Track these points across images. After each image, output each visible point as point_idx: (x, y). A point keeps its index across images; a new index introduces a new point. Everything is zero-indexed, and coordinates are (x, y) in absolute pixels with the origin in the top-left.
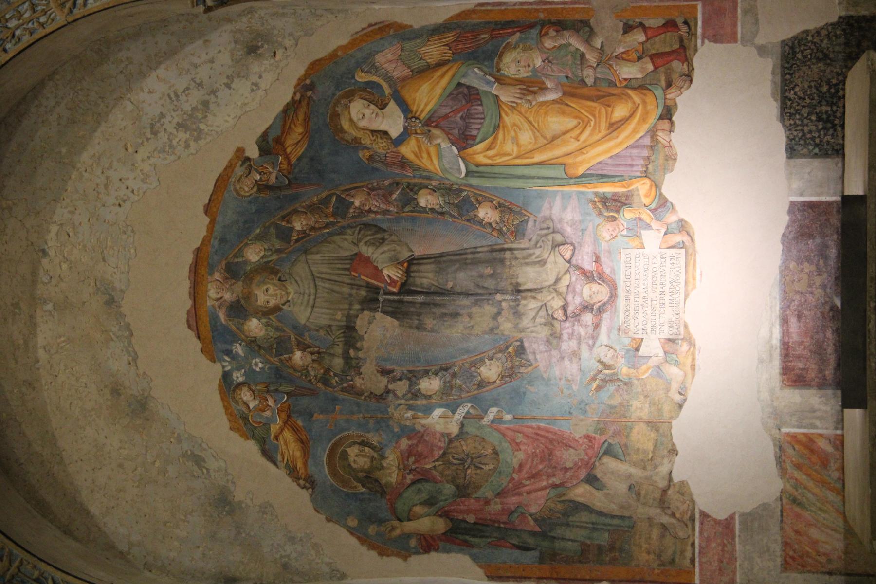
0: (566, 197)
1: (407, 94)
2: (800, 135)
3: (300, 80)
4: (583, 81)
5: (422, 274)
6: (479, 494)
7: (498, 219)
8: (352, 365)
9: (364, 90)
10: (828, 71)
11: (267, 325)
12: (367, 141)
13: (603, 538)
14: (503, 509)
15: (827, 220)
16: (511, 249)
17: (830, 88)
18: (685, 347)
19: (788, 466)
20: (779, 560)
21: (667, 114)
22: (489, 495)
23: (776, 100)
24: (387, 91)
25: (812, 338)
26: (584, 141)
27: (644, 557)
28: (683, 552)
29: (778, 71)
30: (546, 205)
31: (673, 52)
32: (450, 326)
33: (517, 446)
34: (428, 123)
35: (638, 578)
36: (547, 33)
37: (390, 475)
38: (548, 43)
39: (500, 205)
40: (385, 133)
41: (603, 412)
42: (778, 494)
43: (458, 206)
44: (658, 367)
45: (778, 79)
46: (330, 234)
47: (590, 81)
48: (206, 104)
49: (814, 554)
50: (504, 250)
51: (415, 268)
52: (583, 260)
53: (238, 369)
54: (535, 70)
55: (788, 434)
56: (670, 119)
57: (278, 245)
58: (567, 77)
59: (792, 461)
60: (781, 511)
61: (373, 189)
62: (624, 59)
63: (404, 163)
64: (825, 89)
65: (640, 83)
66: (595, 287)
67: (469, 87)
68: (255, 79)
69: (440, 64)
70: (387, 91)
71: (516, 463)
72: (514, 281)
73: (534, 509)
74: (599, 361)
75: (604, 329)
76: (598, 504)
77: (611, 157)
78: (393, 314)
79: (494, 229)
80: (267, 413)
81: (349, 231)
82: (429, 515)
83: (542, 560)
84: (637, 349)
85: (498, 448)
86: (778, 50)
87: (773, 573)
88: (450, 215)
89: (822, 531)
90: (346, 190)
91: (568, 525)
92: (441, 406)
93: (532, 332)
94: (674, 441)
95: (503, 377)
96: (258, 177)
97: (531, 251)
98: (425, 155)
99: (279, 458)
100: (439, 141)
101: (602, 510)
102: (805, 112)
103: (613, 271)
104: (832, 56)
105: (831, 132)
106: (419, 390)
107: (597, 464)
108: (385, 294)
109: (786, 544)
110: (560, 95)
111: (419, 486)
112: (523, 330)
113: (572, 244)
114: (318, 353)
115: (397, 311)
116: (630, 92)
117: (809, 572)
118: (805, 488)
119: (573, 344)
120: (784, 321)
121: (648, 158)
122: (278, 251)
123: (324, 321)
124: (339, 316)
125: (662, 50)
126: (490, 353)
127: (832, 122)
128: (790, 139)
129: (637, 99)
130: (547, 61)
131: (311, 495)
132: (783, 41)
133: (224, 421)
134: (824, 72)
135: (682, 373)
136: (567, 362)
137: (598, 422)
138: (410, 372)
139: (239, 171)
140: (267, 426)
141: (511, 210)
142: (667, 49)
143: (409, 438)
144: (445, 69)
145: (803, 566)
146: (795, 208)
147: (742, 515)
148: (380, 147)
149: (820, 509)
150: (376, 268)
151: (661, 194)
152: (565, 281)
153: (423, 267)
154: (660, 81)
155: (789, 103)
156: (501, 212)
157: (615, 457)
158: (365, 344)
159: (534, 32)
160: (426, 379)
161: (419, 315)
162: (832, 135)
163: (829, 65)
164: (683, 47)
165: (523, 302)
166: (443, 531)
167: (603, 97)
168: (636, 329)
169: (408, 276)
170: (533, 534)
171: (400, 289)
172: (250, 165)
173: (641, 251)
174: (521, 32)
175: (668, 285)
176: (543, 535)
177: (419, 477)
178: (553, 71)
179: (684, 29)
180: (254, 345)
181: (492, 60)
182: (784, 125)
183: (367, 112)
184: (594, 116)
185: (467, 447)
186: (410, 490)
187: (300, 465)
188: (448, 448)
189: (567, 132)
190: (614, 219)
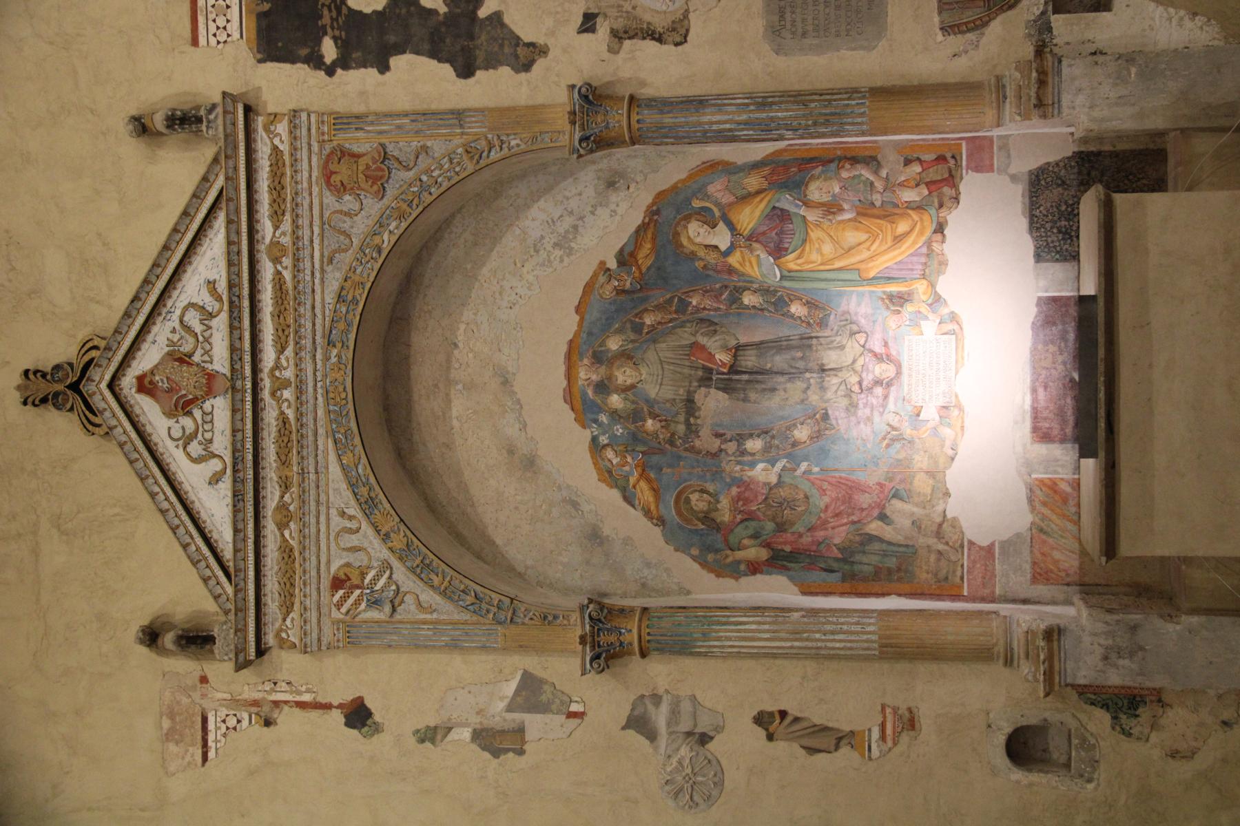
0: (862, 295)
1: (733, 217)
3: (649, 207)
6: (794, 529)
8: (692, 430)
11: (625, 399)
12: (701, 253)
13: (892, 563)
15: (1067, 311)
16: (816, 337)
18: (955, 412)
19: (1037, 504)
20: (1029, 576)
21: (940, 229)
22: (802, 530)
24: (717, 214)
28: (954, 572)
29: (1027, 194)
30: (844, 302)
35: (919, 591)
36: (843, 167)
37: (724, 515)
39: (808, 302)
40: (716, 247)
45: (1027, 200)
46: (674, 328)
47: (878, 204)
48: (575, 227)
50: (812, 338)
51: (741, 353)
54: (834, 196)
55: (1036, 479)
57: (632, 336)
63: (731, 270)
65: (918, 204)
66: (884, 366)
67: (782, 210)
68: (613, 207)
69: (758, 192)
71: (822, 505)
73: (837, 541)
75: (891, 399)
78: (725, 390)
80: (627, 468)
81: (688, 325)
83: (844, 580)
84: (918, 415)
86: (1026, 177)
91: (864, 552)
92: (763, 462)
96: (616, 283)
98: (747, 264)
100: (758, 253)
102: (1048, 226)
103: (899, 353)
104: (1068, 182)
105: (1069, 241)
108: (718, 374)
109: (1034, 563)
111: (746, 523)
113: (866, 333)
114: (666, 420)
116: (910, 212)
120: (1034, 391)
121: (925, 264)
122: (632, 341)
123: (670, 396)
124: (681, 391)
126: (802, 420)
127: (1069, 234)
134: (1063, 194)
136: (862, 425)
137: (888, 472)
139: (602, 279)
140: (626, 478)
142: (939, 178)
143: (738, 487)
144: (762, 196)
145: (1048, 580)
148: (712, 258)
149: (1062, 537)
150: (710, 353)
151: (936, 292)
152: (861, 362)
153: (747, 353)
154: (933, 202)
157: (901, 499)
158: (702, 413)
159: (833, 166)
160: (751, 440)
161: (744, 390)
163: (1065, 189)
164: (951, 175)
165: (827, 379)
174: (823, 165)
176: (844, 560)
177: (746, 516)
179: (952, 162)
180: (615, 415)
181: (800, 188)
182: (1032, 237)
183: (702, 231)
185: (783, 493)
186: (740, 526)
187: (653, 507)
188: (769, 494)
189: (860, 244)
190: (899, 312)
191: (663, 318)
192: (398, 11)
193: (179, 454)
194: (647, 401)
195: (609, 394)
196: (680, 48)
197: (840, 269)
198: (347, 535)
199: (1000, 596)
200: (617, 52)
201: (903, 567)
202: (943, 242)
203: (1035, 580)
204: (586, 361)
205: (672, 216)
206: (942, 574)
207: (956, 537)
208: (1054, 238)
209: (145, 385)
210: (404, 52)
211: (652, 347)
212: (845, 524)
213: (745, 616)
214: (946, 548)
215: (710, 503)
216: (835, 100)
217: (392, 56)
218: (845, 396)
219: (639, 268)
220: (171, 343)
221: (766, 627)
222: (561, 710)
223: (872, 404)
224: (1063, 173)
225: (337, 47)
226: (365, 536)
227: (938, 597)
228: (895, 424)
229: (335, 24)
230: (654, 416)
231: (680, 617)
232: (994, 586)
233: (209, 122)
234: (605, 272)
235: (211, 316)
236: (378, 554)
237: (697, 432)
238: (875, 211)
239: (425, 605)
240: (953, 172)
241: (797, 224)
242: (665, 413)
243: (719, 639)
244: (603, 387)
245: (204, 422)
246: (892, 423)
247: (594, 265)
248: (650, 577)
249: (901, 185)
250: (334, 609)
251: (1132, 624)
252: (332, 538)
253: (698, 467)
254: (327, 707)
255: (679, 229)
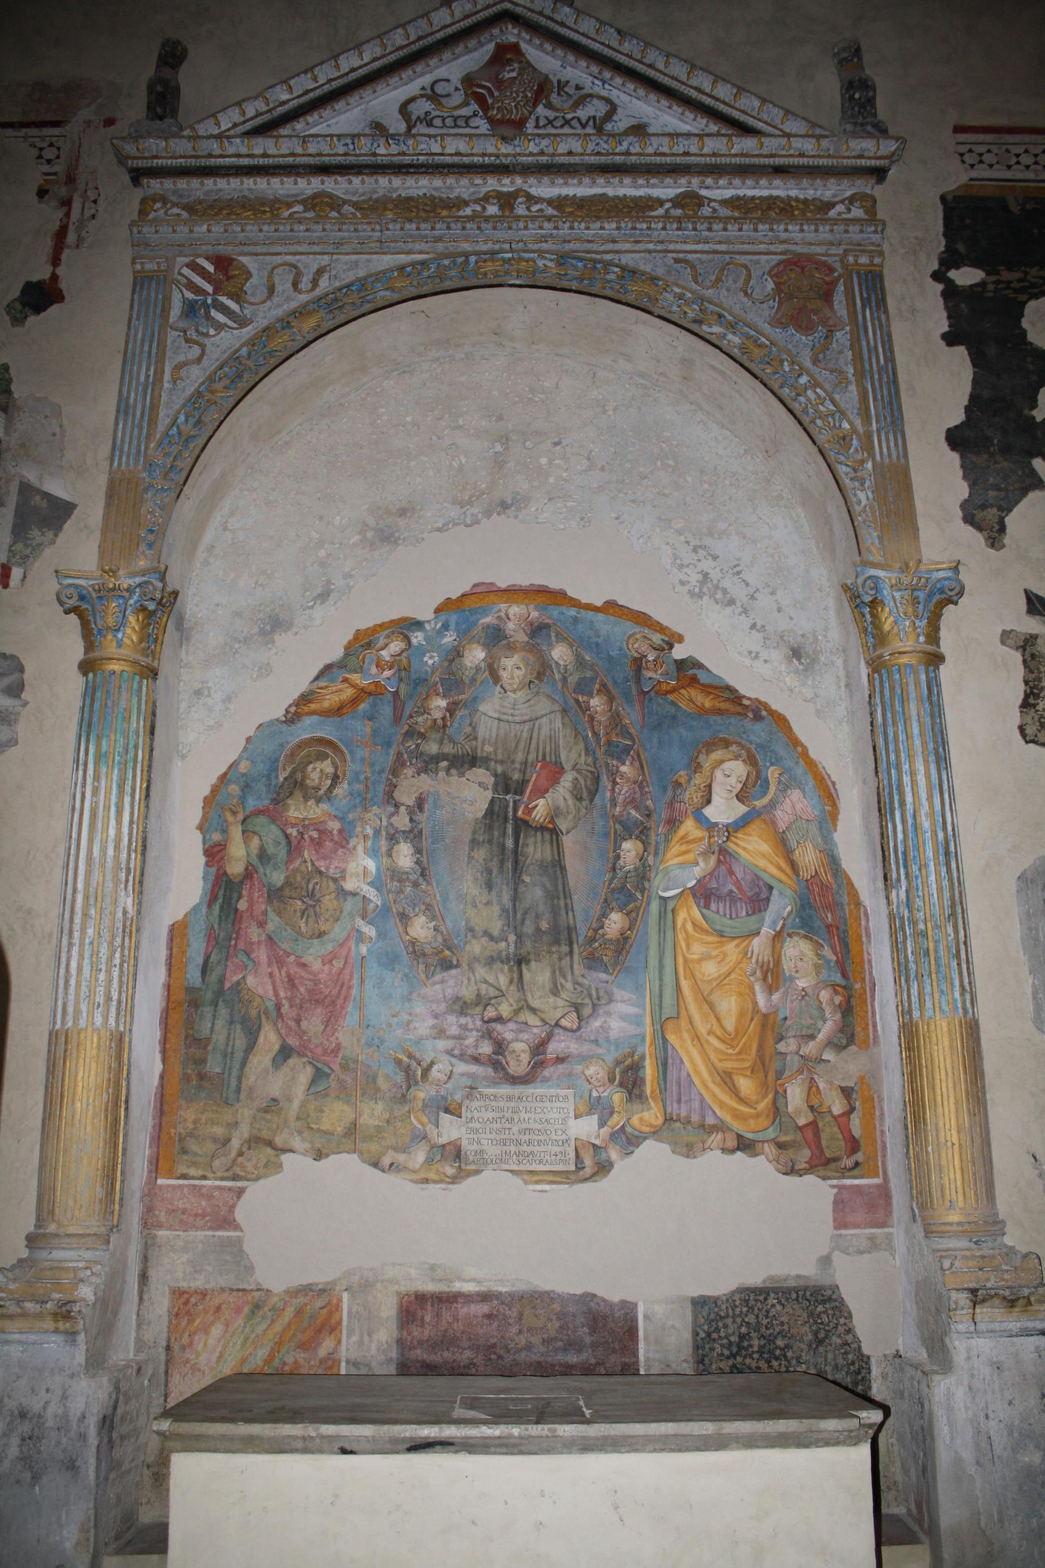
0: (638, 1021)
1: (756, 827)
2: (722, 1314)
3: (766, 706)
4: (781, 1038)
5: (539, 845)
6: (271, 914)
7: (608, 937)
8: (428, 764)
9: (758, 776)
10: (803, 1346)
11: (478, 669)
12: (698, 779)
13: (213, 1066)
14: (252, 944)
15: (614, 1351)
16: (571, 953)
17: (782, 1349)
18: (450, 1171)
19: (301, 1300)
20: (184, 1285)
21: (744, 1145)
22: (270, 927)
23: (764, 1281)
24: (759, 804)
25: (463, 1332)
26: (707, 1041)
27: (190, 1115)
28: (194, 1164)
29: (802, 1283)
30: (627, 995)
31: (822, 1152)
32: (476, 879)
33: (328, 960)
34: (723, 851)
35: (166, 1107)
36: (836, 992)
37: (296, 809)
38: (825, 995)
39: (626, 939)
40: (709, 801)
41: (369, 1067)
42: (265, 1286)
43: (623, 888)
44: (425, 1137)
45: (791, 1283)
46: (585, 738)
47: (781, 1047)
48: (731, 602)
49: (192, 1328)
50: (571, 945)
51: (547, 836)
52: (560, 1041)
53: (425, 639)
54: (792, 979)
55: (340, 1300)
56: (738, 1149)
57: (573, 679)
58: (785, 1019)
59: (306, 1305)
60: (244, 1290)
61: (641, 787)
62: (810, 1088)
63: (673, 823)
64: (780, 1342)
65: (782, 1109)
66: (525, 1057)
67: (768, 899)
68: (764, 654)
69: (793, 865)
70: (759, 804)
71: (307, 959)
72: (532, 956)
73: (251, 980)
74: (432, 1063)
75: (473, 1068)
76: (255, 1061)
77: (689, 1075)
78: (490, 812)
79: (596, 931)
80: (374, 670)
81: (590, 760)
82: (248, 855)
83: (190, 990)
84: (447, 1111)
85: (326, 937)
86: (827, 1281)
87: (169, 1276)
88: (613, 879)
89: (219, 1340)
90: (639, 756)
91: (231, 1023)
92: (378, 870)
93: (469, 979)
94: (333, 1157)
95: (413, 943)
96: (651, 658)
97: (569, 977)
98: (684, 848)
99: (322, 684)
100: (702, 864)
101: (248, 1065)
102: (751, 1319)
103: (546, 1080)
104: (821, 1349)
105: (727, 1352)
106: (398, 843)
107: (305, 1059)
108: (515, 802)
109: (204, 1294)
110: (764, 1010)
111: (284, 842)
112: (471, 968)
113: (579, 1028)
114: (445, 726)
115: (494, 814)
116: (770, 1096)
117: (170, 1322)
118: (273, 1321)
119: (454, 1030)
120: (485, 1297)
121: (689, 1122)
122: (564, 680)
123: (481, 733)
124: (488, 749)
125: (824, 1137)
126: (442, 928)
127: (737, 1353)
128: (715, 1301)
129: (762, 1106)
130: (804, 994)
131: (277, 720)
132: (837, 1287)
133: (366, 623)
134: (801, 1341)
135: (417, 1166)
136: (431, 1022)
137: (356, 1061)
138: (421, 832)
139: (657, 638)
140: (360, 670)
141: (620, 953)
142: (824, 1143)
143: (340, 831)
144: (788, 870)
145: (177, 1315)
146: (628, 1310)
147: (240, 1241)
148: (692, 795)
149: (247, 1338)
150: (547, 791)
151: (645, 1138)
152: (532, 1020)
153: (548, 845)
154: (786, 1134)
155: (761, 1298)
156: (618, 940)
157: (313, 1082)
158: (454, 779)
159: (838, 978)
160: (412, 851)
161: (490, 842)
162: (722, 1354)
163: (810, 1346)
164: (828, 1162)
165: (506, 968)
166: (229, 872)
167: (763, 1065)
168: (473, 1109)
169: (536, 829)
170: (221, 980)
171: (522, 820)
172: (663, 650)
173: (572, 1114)
174: (837, 962)
175: (531, 1148)
176: (220, 993)
177: (294, 842)
178: (792, 1001)
179: (849, 1162)
180: (456, 654)
181: (802, 928)
182: (733, 1293)
183: (733, 780)
184: (739, 1053)
185: (328, 902)
186: (279, 833)
187: (313, 706)
188: (327, 877)
189: (718, 1019)
190: (611, 1080)
191: (600, 723)
192: (1029, 360)
193: (413, 88)
194: (475, 699)
195: (486, 646)
196: (1017, 732)
197: (678, 989)
198: (292, 277)
199: (154, 1237)
200: (1003, 643)
201: (206, 1084)
202: (724, 1150)
203: (178, 1293)
204: (534, 614)
205: (752, 738)
206: (193, 1146)
207: (250, 1169)
208: (731, 1329)
209: (506, 54)
210: (974, 365)
211: (556, 707)
212: (276, 994)
213: (131, 822)
214: (234, 1153)
215: (317, 789)
216: (959, 964)
217: (968, 349)
218: (478, 995)
219: (674, 690)
220: (562, 85)
221: (110, 852)
222: (14, 556)
223: (466, 1038)
224: (836, 1340)
225: (972, 286)
226: (288, 299)
227: (158, 1138)
228: (434, 1072)
229: (1001, 286)
230: (451, 710)
231: (137, 724)
232: (170, 1228)
233: (862, 125)
234: (667, 643)
235: (600, 130)
236: (261, 315)
237: (425, 770)
238: (770, 1041)
239: (183, 373)
240: (833, 1165)
241: (745, 922)
242: (456, 725)
243: (97, 777)
244: (495, 637)
245: (456, 119)
246: (435, 1068)
247: (676, 628)
248: (210, 702)
249: (812, 1083)
250: (186, 260)
251: (78, 1464)
252: (289, 258)
253: (373, 772)
254: (56, 261)
255: (734, 748)
